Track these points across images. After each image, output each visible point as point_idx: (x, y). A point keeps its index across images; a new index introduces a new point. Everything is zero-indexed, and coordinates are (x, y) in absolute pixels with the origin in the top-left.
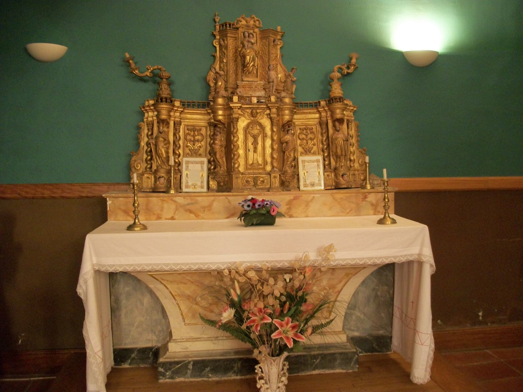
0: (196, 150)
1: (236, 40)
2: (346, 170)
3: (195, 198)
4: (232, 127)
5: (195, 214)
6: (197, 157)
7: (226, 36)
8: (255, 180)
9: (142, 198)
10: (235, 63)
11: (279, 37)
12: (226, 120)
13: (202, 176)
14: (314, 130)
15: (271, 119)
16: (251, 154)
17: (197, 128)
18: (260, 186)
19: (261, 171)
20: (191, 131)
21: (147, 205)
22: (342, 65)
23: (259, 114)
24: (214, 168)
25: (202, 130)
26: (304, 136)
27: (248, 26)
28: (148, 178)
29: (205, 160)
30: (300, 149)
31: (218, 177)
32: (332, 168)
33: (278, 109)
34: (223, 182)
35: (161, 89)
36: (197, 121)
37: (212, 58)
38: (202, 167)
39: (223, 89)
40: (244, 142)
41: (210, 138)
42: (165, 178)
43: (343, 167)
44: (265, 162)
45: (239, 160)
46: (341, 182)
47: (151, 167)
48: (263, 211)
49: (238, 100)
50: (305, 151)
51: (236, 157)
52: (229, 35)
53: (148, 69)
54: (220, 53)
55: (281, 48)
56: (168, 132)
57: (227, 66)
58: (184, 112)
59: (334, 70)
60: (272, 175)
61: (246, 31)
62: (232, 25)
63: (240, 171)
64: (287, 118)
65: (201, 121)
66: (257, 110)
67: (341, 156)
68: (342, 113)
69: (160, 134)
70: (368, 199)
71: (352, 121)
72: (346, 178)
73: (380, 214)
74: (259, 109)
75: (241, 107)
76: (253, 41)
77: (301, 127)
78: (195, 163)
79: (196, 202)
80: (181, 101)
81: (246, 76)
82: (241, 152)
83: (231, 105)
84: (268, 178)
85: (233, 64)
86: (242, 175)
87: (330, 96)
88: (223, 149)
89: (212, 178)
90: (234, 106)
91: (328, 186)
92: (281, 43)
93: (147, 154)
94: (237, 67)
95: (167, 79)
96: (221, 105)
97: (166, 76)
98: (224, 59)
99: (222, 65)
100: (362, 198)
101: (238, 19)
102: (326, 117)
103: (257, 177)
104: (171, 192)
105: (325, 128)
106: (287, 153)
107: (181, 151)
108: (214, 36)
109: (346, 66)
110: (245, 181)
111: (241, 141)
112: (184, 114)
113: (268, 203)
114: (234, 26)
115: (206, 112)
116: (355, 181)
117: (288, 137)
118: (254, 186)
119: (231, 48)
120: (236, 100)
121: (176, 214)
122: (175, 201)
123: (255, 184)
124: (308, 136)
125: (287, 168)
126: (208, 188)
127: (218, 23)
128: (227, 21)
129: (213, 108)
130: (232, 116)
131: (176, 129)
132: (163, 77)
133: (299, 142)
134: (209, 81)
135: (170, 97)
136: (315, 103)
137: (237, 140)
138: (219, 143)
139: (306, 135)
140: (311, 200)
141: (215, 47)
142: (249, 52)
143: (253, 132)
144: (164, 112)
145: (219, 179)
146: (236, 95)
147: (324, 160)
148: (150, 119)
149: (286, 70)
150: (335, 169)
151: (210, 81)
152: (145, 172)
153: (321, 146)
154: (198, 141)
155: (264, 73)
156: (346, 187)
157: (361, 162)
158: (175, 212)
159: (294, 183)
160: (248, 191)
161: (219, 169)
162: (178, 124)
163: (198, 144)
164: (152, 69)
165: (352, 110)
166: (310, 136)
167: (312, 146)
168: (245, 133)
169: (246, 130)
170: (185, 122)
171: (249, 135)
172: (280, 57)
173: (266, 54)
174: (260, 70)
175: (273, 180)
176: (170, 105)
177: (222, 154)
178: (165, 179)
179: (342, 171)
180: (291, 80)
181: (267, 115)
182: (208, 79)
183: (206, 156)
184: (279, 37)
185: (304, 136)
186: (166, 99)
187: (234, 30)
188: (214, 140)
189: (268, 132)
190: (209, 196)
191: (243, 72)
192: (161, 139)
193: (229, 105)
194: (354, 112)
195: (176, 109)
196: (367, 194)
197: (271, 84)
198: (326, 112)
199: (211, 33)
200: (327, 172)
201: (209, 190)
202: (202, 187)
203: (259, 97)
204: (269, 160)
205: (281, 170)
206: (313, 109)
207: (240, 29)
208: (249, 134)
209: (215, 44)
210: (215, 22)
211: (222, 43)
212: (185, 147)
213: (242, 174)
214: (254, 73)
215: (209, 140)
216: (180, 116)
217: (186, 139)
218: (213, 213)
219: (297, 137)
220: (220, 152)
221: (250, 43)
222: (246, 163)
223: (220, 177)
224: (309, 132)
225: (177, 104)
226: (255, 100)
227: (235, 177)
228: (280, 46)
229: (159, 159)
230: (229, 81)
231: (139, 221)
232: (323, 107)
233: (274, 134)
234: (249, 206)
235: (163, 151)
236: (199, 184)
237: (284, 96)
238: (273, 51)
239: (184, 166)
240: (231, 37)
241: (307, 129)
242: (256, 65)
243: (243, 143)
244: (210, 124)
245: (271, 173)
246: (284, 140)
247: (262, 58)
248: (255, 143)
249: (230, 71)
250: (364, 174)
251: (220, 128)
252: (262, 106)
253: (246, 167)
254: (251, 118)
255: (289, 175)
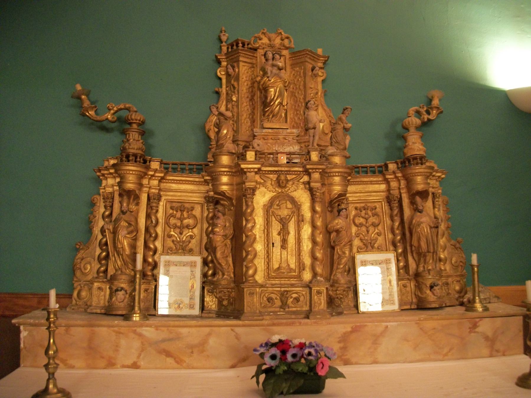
0: (184, 242)
1: (253, 67)
2: (437, 278)
3: (176, 329)
4: (244, 204)
5: (175, 359)
6: (184, 255)
7: (238, 61)
8: (284, 296)
9: (82, 328)
10: (251, 103)
11: (320, 65)
12: (235, 192)
13: (193, 287)
14: (378, 210)
15: (311, 190)
16: (276, 251)
17: (187, 205)
18: (292, 307)
19: (293, 281)
20: (177, 211)
21: (90, 340)
22: (420, 107)
23: (291, 183)
24: (214, 274)
25: (195, 209)
26: (362, 220)
27: (271, 46)
28: (100, 288)
29: (198, 260)
30: (357, 242)
31: (218, 292)
32: (411, 273)
33: (324, 174)
34: (227, 299)
35: (128, 140)
36: (187, 194)
37: (215, 96)
38: (192, 271)
39: (230, 141)
40: (264, 231)
41: (208, 222)
42: (126, 291)
43: (432, 273)
44: (301, 264)
45: (256, 262)
46: (429, 297)
47: (106, 271)
48: (302, 368)
49: (256, 159)
50: (364, 244)
51: (249, 257)
52: (241, 59)
53: (110, 110)
54: (227, 87)
55: (323, 80)
56: (138, 212)
57: (237, 106)
58: (165, 179)
59: (408, 113)
60: (313, 288)
61: (269, 51)
62: (246, 44)
63: (256, 282)
64: (337, 189)
65: (194, 195)
66: (288, 176)
67: (427, 254)
68: (425, 181)
69: (122, 215)
70: (479, 329)
71: (439, 196)
72: (438, 291)
73: (500, 356)
74: (291, 174)
75: (259, 169)
76: (280, 64)
77: (358, 205)
78: (180, 266)
79: (178, 337)
80: (162, 161)
81: (268, 121)
82: (259, 247)
83: (243, 166)
84: (306, 293)
85: (248, 104)
86: (260, 288)
87: (404, 154)
88: (228, 242)
89: (208, 292)
90: (247, 168)
91: (405, 304)
92: (323, 73)
93: (101, 248)
94: (254, 109)
95: (139, 125)
96: (225, 167)
97: (136, 120)
98: (234, 96)
99: (230, 106)
100: (470, 328)
101: (256, 35)
102: (399, 189)
103: (287, 291)
104: (134, 319)
105: (397, 207)
106: (338, 249)
107: (158, 244)
108: (219, 62)
109: (425, 109)
110: (265, 299)
111: (260, 229)
112: (167, 182)
113: (312, 351)
114: (250, 46)
115: (202, 180)
116: (448, 294)
117: (339, 222)
118: (281, 307)
119: (245, 78)
120: (251, 158)
121: (141, 357)
122: (140, 335)
123: (284, 305)
124: (369, 220)
125: (339, 275)
126: (202, 308)
127: (226, 42)
128: (239, 38)
129: (212, 172)
130: (244, 186)
131: (151, 207)
132: (131, 121)
133: (354, 229)
134: (209, 131)
135: (142, 154)
136: (379, 167)
137: (253, 227)
138: (222, 232)
139: (365, 218)
140: (383, 334)
141: (220, 79)
142: (275, 82)
143: (280, 213)
144: (130, 178)
145: (220, 295)
146: (251, 149)
147: (398, 261)
148: (110, 190)
149: (332, 115)
150: (417, 275)
151: (210, 131)
152: (96, 278)
153: (390, 236)
154: (188, 227)
155: (296, 118)
156: (437, 306)
157: (456, 262)
158: (140, 355)
159: (349, 301)
160: (271, 317)
161: (221, 277)
162: (154, 199)
163: (188, 233)
164: (115, 109)
165: (439, 177)
166: (372, 220)
167: (376, 236)
168: (267, 214)
169: (268, 208)
170: (166, 195)
171: (274, 219)
172: (323, 95)
173: (300, 89)
174: (290, 115)
175: (316, 297)
176: (141, 167)
177: (226, 251)
178: (127, 293)
179: (429, 279)
180: (344, 126)
181: (304, 183)
182: (207, 128)
183: (200, 253)
184: (320, 65)
185: (362, 220)
186: (135, 155)
187: (250, 52)
188: (214, 225)
189: (306, 211)
190: (200, 326)
191: (264, 115)
192: (124, 224)
193: (239, 165)
194: (441, 180)
195: (151, 173)
196: (477, 320)
197: (312, 131)
198: (399, 181)
199: (214, 58)
200: (402, 280)
201: (204, 312)
202: (192, 307)
203: (290, 154)
204: (307, 261)
205: (328, 279)
206: (377, 177)
207: (259, 50)
208: (273, 217)
209: (219, 74)
210: (221, 42)
211: (231, 70)
212: (166, 237)
213: (262, 286)
214: (281, 116)
215: (205, 225)
216: (159, 186)
217: (167, 224)
218: (208, 356)
219: (352, 221)
220: (223, 247)
221: (276, 68)
222: (268, 268)
223: (222, 291)
224: (370, 213)
225: (155, 165)
226: (283, 159)
227: (248, 292)
228: (322, 78)
229: (119, 257)
230: (240, 130)
231: (55, 385)
232: (394, 173)
233: (318, 216)
234: (273, 357)
235: (126, 244)
236: (187, 301)
237: (332, 153)
238: (311, 84)
239: (162, 269)
240: (245, 62)
241: (368, 209)
242: (285, 103)
243: (262, 232)
244: (208, 200)
245: (311, 285)
246: (334, 226)
247: (293, 95)
248: (284, 232)
249: (243, 115)
250: (460, 281)
251: (223, 205)
252: (297, 169)
253: (268, 273)
254: (277, 189)
255: (342, 288)
